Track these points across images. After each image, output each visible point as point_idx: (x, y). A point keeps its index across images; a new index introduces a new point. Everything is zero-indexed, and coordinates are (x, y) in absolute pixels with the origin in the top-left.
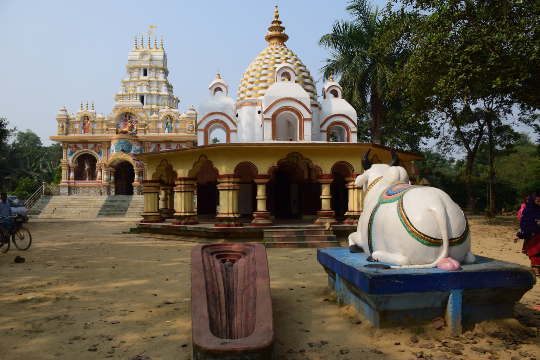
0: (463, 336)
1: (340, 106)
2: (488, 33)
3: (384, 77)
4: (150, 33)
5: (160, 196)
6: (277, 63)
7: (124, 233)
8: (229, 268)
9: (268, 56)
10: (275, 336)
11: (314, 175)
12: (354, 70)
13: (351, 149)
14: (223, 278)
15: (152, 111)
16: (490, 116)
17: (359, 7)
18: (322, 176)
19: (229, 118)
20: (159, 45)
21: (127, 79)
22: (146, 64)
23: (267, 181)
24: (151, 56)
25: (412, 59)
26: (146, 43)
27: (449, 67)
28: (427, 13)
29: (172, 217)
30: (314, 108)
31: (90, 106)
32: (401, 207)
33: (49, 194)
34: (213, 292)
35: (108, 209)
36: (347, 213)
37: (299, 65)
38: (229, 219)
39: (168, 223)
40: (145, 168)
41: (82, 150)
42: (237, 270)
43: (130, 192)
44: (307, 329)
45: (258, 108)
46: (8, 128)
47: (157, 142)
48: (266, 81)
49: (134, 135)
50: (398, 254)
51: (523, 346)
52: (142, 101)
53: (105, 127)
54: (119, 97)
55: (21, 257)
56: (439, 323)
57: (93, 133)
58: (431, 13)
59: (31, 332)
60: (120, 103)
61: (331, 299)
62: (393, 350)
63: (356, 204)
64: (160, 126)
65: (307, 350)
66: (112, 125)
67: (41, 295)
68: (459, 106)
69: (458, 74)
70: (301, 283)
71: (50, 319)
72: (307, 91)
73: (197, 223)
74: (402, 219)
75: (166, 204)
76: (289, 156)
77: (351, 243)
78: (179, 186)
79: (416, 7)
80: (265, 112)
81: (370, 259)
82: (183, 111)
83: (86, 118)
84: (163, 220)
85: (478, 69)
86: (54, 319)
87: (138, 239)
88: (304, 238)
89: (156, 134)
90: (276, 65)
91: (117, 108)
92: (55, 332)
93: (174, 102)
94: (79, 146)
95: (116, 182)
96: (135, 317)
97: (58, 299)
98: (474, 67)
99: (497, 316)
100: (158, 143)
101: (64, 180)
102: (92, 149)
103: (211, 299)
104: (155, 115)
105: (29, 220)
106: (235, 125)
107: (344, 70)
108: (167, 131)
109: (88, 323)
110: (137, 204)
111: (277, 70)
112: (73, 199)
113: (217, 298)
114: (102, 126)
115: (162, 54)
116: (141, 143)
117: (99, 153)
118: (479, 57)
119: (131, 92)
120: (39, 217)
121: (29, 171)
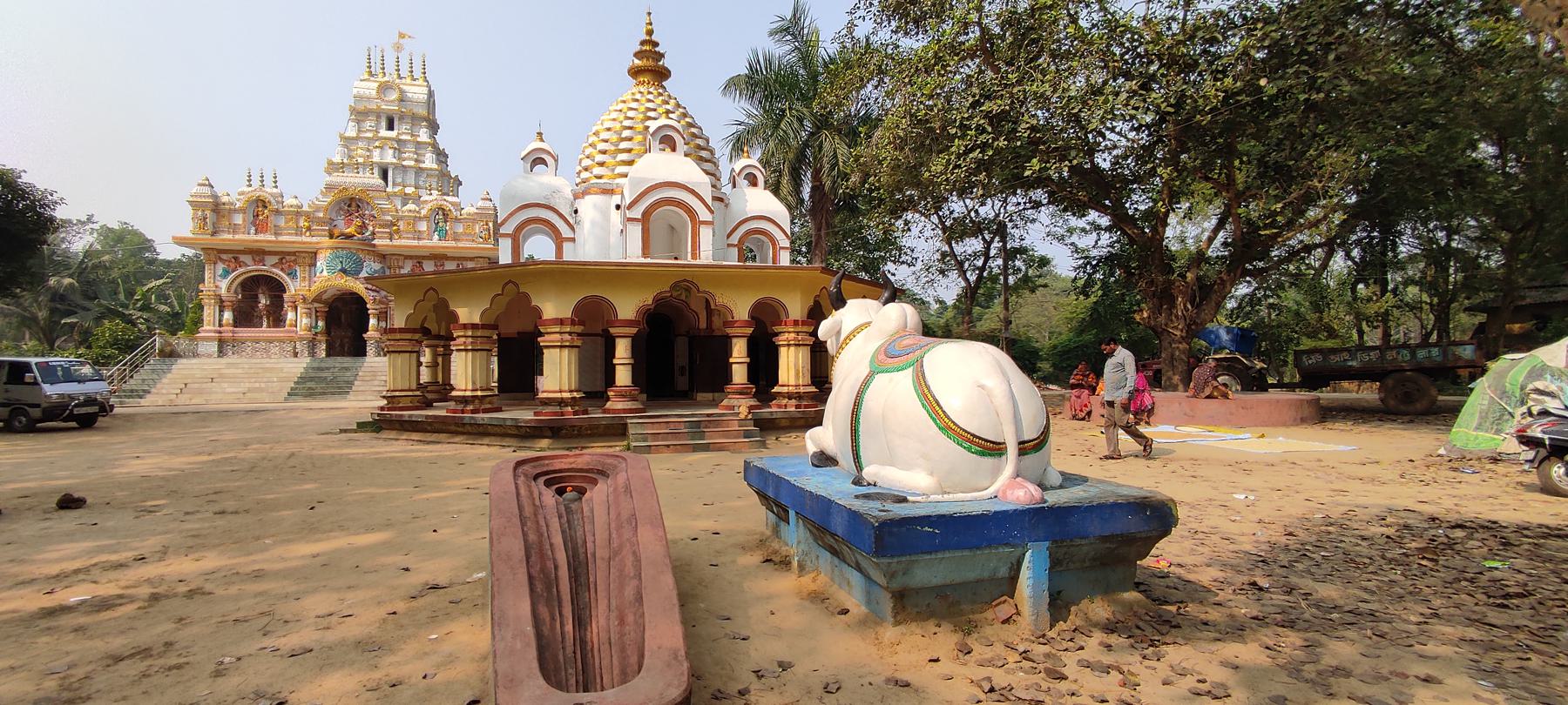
0: (1051, 634)
1: (761, 202)
2: (1019, 82)
3: (835, 156)
4: (398, 48)
6: (650, 118)
7: (342, 431)
8: (574, 506)
9: (634, 105)
14: (563, 532)
15: (406, 199)
18: (731, 324)
20: (418, 73)
21: (352, 133)
22: (390, 104)
23: (634, 330)
24: (402, 92)
25: (887, 121)
27: (952, 138)
28: (913, 44)
30: (717, 203)
31: (269, 181)
32: (921, 382)
33: (170, 354)
34: (543, 570)
35: (309, 385)
36: (776, 389)
37: (691, 125)
38: (561, 402)
39: (439, 411)
40: (392, 305)
41: (251, 268)
42: (592, 511)
43: (359, 350)
44: (744, 633)
45: (616, 199)
46: (60, 213)
47: (417, 257)
48: (629, 151)
49: (368, 243)
50: (916, 472)
51: (1169, 649)
52: (384, 176)
53: (303, 223)
54: (333, 167)
55: (76, 495)
56: (1005, 610)
58: (921, 44)
60: (337, 178)
61: (777, 559)
62: (922, 676)
63: (792, 373)
64: (423, 226)
65: (752, 688)
66: (321, 222)
67: (107, 589)
68: (957, 206)
69: (968, 151)
70: (709, 524)
71: (118, 659)
72: (707, 173)
73: (499, 410)
74: (921, 405)
75: (435, 374)
76: (675, 286)
77: (812, 449)
78: (461, 339)
79: (896, 32)
80: (630, 207)
81: (858, 482)
82: (469, 201)
83: (261, 203)
84: (428, 405)
86: (132, 656)
88: (702, 435)
89: (415, 243)
90: (648, 123)
91: (329, 188)
92: (124, 698)
93: (450, 183)
94: (246, 259)
95: (328, 330)
96: (352, 630)
97: (155, 598)
98: (994, 140)
99: (1107, 590)
100: (419, 259)
101: (208, 327)
103: (539, 587)
105: (116, 410)
106: (573, 229)
107: (766, 140)
108: (436, 237)
109: (227, 660)
110: (374, 374)
111: (651, 130)
113: (551, 583)
115: (425, 90)
116: (383, 257)
117: (293, 275)
118: (996, 120)
119: (361, 160)
120: (147, 401)
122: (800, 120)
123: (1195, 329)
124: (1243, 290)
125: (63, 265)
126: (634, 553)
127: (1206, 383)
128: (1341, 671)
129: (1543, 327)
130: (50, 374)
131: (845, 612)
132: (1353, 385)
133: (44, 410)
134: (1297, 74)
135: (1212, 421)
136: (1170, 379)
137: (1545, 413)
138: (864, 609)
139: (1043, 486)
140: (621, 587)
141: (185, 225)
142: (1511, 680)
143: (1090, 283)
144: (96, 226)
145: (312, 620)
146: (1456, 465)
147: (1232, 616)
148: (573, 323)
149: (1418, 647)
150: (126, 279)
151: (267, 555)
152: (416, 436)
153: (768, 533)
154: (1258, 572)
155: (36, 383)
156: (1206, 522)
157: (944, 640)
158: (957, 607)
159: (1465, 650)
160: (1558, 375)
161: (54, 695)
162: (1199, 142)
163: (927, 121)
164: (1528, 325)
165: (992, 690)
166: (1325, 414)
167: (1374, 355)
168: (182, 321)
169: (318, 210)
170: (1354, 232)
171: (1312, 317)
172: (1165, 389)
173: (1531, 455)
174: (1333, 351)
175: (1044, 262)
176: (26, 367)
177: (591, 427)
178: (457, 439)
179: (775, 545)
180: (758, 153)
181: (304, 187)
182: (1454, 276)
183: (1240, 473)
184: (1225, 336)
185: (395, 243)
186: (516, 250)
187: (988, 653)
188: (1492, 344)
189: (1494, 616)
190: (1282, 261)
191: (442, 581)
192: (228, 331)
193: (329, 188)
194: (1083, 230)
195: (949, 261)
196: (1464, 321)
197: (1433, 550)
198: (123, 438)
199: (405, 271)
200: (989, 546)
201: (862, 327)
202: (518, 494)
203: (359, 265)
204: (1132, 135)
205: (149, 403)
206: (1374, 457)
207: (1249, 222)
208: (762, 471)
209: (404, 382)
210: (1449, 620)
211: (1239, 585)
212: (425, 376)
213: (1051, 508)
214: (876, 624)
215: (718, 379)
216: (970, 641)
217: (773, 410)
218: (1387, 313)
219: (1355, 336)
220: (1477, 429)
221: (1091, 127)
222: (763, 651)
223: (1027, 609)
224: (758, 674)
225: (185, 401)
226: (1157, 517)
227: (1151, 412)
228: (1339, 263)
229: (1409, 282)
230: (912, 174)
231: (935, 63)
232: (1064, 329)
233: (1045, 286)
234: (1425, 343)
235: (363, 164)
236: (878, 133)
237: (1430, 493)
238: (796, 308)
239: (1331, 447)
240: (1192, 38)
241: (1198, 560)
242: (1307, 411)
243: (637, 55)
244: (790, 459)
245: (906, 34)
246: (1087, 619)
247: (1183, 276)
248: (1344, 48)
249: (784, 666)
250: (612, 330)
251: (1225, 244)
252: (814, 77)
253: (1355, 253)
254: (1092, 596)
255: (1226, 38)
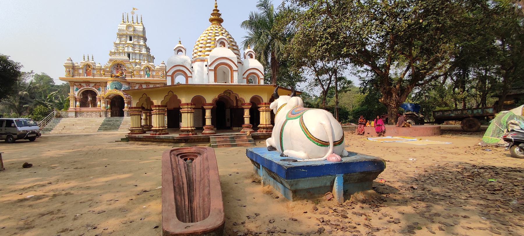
0: (344, 204)
1: (254, 63)
2: (339, 22)
3: (279, 47)
5: (142, 117)
6: (216, 36)
7: (116, 141)
9: (211, 31)
10: (226, 216)
11: (239, 104)
12: (262, 43)
13: (260, 88)
14: (186, 173)
15: (136, 64)
16: (335, 71)
17: (264, 5)
18: (244, 104)
19: (187, 69)
20: (139, 21)
21: (118, 42)
22: (130, 32)
23: (212, 107)
24: (134, 28)
25: (296, 36)
26: (130, 19)
27: (317, 41)
28: (305, 9)
29: (150, 130)
30: (239, 64)
31: (90, 58)
32: (302, 123)
33: (59, 117)
34: (179, 185)
35: (105, 126)
37: (230, 38)
39: (148, 134)
41: (85, 87)
42: (195, 166)
43: (122, 115)
44: (244, 205)
45: (206, 63)
46: (22, 70)
48: (210, 47)
49: (124, 79)
51: (382, 208)
52: (129, 56)
53: (102, 72)
54: (112, 53)
56: (329, 196)
57: (93, 76)
58: (307, 9)
59: (21, 229)
60: (113, 57)
61: (256, 181)
63: (264, 120)
64: (142, 73)
66: (108, 72)
67: (39, 193)
68: (320, 64)
70: (236, 170)
72: (236, 54)
73: (168, 134)
74: (302, 130)
75: (146, 122)
76: (225, 92)
77: (268, 145)
78: (155, 111)
79: (299, 6)
81: (282, 155)
82: (157, 64)
83: (88, 66)
84: (144, 132)
85: (334, 42)
86: (48, 214)
87: (127, 145)
88: (234, 141)
89: (139, 78)
90: (216, 37)
91: (111, 60)
92: (45, 227)
93: (151, 58)
95: (111, 108)
96: (118, 205)
97: (55, 196)
99: (363, 190)
100: (141, 84)
101: (72, 107)
102: (93, 87)
103: (177, 190)
104: (138, 66)
105: (42, 135)
109: (78, 215)
110: (127, 122)
111: (217, 40)
112: (79, 120)
113: (181, 188)
114: (100, 72)
115: (142, 27)
116: (129, 83)
118: (333, 36)
119: (121, 51)
121: (44, 101)
122: (267, 35)
123: (399, 104)
124: (417, 91)
125: (24, 87)
126: (208, 179)
127: (402, 122)
128: (437, 215)
129: (517, 101)
130: (20, 123)
131: (278, 197)
132: (453, 122)
133: (18, 136)
134: (432, 18)
135: (405, 135)
136: (391, 121)
137: (513, 131)
138: (283, 196)
139: (342, 156)
140: (204, 190)
141: (63, 73)
142: (492, 216)
143: (365, 89)
144: (34, 74)
145: (105, 202)
146: (484, 148)
147: (404, 198)
148: (191, 104)
149: (463, 207)
150: (45, 91)
151: (91, 182)
152: (140, 143)
153: (254, 173)
154: (414, 183)
155: (15, 127)
156: (399, 168)
157: (309, 206)
158: (313, 195)
159: (479, 208)
160: (518, 118)
161: (23, 226)
162: (401, 42)
163: (309, 35)
164: (512, 101)
165: (323, 221)
166: (442, 132)
167: (459, 112)
168: (63, 105)
169: (107, 68)
170: (454, 71)
171: (440, 100)
172: (389, 124)
173: (508, 144)
174: (446, 111)
175: (350, 82)
176: (12, 121)
177: (198, 139)
178: (154, 144)
179: (257, 177)
180: (253, 47)
181: (102, 60)
182: (488, 84)
183: (407, 151)
184: (409, 106)
185: (133, 78)
186: (173, 81)
187: (323, 210)
188: (499, 107)
189: (490, 197)
190: (430, 80)
191: (147, 189)
192: (78, 109)
193: (111, 60)
194: (363, 71)
195: (318, 82)
196: (491, 101)
197: (472, 176)
198: (44, 144)
199: (136, 88)
200: (323, 175)
201: (285, 104)
202: (171, 161)
203: (121, 86)
204: (378, 39)
205: (53, 133)
206: (457, 146)
207: (417, 68)
208: (252, 152)
209: (136, 125)
210: (475, 198)
211: (407, 188)
212: (143, 123)
213: (344, 163)
214: (287, 201)
215: (240, 123)
216: (318, 206)
217: (258, 133)
218: (465, 98)
219: (454, 106)
220: (492, 136)
221: (364, 37)
222: (250, 210)
223: (336, 196)
224: (248, 217)
225: (65, 132)
226: (379, 166)
227: (384, 132)
228: (449, 81)
229: (472, 87)
230: (304, 53)
231: (311, 16)
232: (357, 104)
233: (350, 90)
234: (477, 108)
235: (122, 52)
236: (293, 40)
237: (474, 157)
238: (265, 99)
239: (444, 143)
240: (397, 6)
241: (395, 180)
242: (436, 131)
243: (212, 14)
244: (261, 150)
245: (302, 6)
246: (356, 199)
247: (395, 87)
248: (448, 9)
249: (257, 215)
250: (204, 107)
251: (409, 76)
252: (272, 21)
253: (455, 78)
254: (358, 191)
255: (409, 6)
